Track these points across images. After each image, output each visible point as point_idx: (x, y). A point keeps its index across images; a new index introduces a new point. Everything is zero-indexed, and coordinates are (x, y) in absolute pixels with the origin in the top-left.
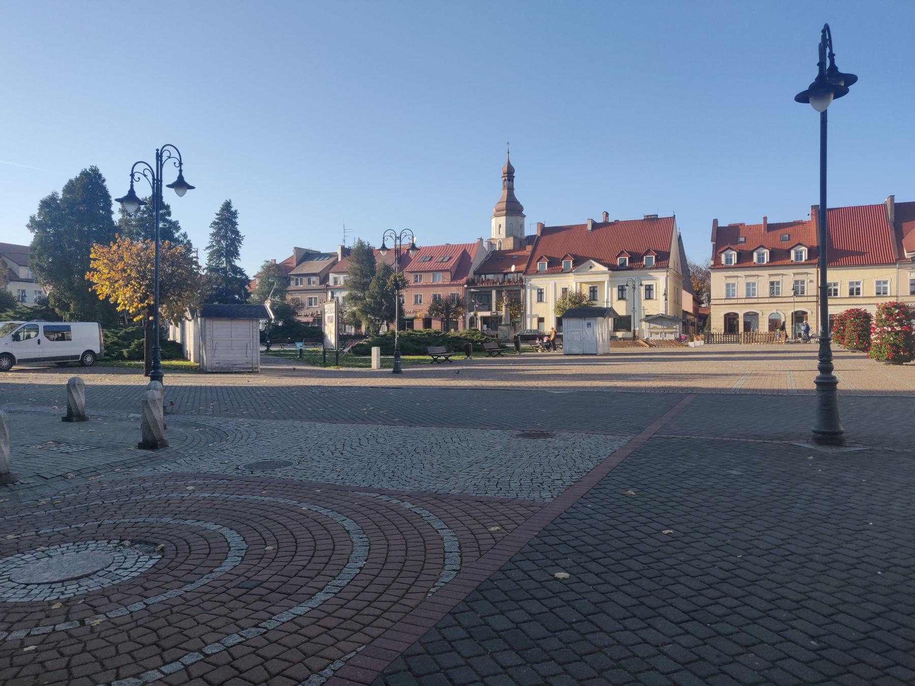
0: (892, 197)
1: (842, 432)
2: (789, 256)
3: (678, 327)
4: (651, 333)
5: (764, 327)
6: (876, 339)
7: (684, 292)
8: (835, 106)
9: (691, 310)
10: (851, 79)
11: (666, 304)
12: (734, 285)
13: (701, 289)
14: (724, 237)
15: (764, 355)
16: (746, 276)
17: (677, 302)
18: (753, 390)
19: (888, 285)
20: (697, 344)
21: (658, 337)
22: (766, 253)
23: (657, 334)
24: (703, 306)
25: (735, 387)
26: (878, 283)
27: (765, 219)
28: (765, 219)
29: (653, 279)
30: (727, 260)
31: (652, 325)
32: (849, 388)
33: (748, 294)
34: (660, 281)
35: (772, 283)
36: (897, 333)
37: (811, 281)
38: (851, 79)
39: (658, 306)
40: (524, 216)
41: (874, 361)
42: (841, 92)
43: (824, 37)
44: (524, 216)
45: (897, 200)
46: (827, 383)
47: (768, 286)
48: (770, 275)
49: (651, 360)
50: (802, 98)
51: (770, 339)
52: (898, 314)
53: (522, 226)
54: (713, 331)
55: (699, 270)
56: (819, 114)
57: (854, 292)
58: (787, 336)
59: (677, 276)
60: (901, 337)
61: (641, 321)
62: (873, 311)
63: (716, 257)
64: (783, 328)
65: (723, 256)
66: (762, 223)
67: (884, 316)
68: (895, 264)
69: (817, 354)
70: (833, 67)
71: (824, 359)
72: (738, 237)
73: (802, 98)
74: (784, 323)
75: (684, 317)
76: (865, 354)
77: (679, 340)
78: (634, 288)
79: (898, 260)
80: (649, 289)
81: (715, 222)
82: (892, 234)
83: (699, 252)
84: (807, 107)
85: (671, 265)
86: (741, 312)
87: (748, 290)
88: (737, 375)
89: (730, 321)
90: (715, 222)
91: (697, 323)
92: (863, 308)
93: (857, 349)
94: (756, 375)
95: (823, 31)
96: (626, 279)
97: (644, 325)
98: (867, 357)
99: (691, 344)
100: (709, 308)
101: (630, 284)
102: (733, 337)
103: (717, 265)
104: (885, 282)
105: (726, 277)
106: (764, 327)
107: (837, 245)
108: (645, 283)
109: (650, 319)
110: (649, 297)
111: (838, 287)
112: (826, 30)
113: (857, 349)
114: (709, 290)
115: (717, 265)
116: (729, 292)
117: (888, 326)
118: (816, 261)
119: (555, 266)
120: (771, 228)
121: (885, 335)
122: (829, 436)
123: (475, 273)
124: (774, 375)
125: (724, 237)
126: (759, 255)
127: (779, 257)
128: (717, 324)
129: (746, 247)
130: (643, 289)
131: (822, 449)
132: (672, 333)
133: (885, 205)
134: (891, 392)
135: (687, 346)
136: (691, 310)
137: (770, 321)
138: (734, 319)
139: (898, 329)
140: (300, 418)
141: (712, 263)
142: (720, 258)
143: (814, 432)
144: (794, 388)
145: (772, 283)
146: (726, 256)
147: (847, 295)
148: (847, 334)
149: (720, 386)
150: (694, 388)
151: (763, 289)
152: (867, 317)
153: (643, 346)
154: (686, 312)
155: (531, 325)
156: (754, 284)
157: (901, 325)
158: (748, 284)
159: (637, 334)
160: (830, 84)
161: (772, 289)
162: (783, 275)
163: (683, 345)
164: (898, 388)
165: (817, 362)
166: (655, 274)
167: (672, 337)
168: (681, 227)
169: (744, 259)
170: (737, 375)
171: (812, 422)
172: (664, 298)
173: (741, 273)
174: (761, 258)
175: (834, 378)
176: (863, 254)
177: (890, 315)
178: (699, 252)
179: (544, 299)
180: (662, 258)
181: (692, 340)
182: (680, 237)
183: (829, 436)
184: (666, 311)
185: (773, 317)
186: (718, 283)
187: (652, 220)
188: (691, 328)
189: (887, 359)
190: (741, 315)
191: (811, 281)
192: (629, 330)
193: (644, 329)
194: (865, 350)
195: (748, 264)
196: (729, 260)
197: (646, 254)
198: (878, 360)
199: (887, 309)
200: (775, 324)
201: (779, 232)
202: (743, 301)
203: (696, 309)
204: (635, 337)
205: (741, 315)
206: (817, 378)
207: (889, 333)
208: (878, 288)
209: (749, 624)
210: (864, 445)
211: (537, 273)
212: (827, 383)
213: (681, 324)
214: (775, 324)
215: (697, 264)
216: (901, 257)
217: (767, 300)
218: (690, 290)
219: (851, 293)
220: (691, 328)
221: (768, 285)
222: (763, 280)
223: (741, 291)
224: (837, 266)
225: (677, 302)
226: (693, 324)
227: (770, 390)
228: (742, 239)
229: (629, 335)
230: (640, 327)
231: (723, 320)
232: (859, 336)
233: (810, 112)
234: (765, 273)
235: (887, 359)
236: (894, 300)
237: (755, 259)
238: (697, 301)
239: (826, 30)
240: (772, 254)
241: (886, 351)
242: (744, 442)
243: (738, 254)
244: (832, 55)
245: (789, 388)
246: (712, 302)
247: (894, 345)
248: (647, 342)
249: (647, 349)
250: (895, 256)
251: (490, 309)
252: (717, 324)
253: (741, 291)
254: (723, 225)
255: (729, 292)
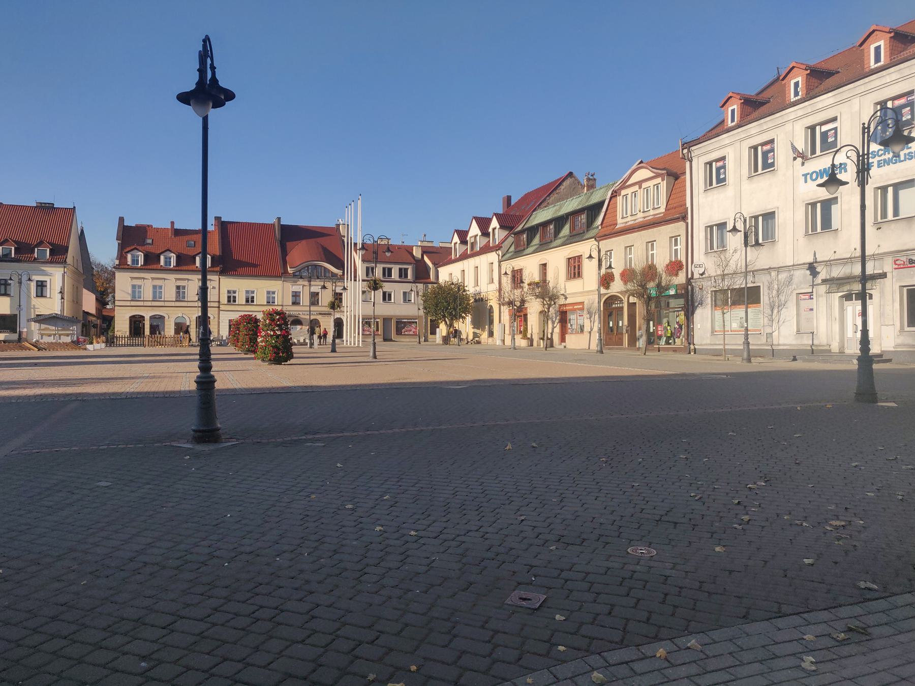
0: (279, 219)
1: (218, 429)
2: (194, 262)
3: (75, 329)
4: (42, 335)
5: (169, 330)
6: (262, 342)
7: (85, 291)
8: (214, 114)
9: (93, 311)
10: (230, 96)
11: (63, 303)
12: (140, 287)
13: (106, 289)
14: (131, 237)
15: (188, 357)
16: (153, 279)
17: (77, 301)
18: (146, 393)
19: (276, 295)
20: (97, 347)
21: (51, 340)
22: (173, 257)
23: (50, 336)
24: (108, 307)
25: (128, 390)
26: (268, 293)
27: (172, 223)
28: (172, 223)
29: (47, 275)
30: (133, 261)
31: (43, 326)
32: (236, 387)
33: (154, 296)
34: (56, 277)
35: (178, 287)
36: (278, 336)
37: (214, 288)
38: (230, 96)
39: (52, 305)
41: (259, 361)
42: (218, 104)
43: (205, 46)
45: (284, 222)
46: (206, 382)
47: (174, 290)
48: (177, 279)
49: (36, 365)
50: (184, 98)
51: (177, 342)
52: (278, 320)
54: (117, 334)
55: (104, 269)
56: (201, 119)
57: (250, 300)
58: (190, 340)
59: (76, 272)
60: (281, 339)
61: (29, 321)
62: (260, 316)
63: (122, 257)
64: (187, 332)
65: (129, 257)
67: (268, 322)
68: (280, 277)
69: (212, 357)
70: (214, 79)
71: (204, 358)
72: (145, 238)
73: (184, 98)
74: (188, 326)
75: (85, 318)
76: (253, 356)
77: (76, 344)
78: (20, 283)
79: (282, 274)
80: (41, 285)
81: (121, 220)
82: (279, 250)
83: (104, 251)
84: (188, 111)
85: (69, 260)
86: (147, 314)
87: (154, 293)
88: (133, 378)
89: (136, 324)
90: (121, 220)
91: (99, 325)
92: (254, 314)
93: (249, 351)
94: (154, 377)
95: (204, 41)
96: (10, 272)
97: (34, 326)
98: (254, 358)
99: (89, 347)
100: (113, 310)
101: (15, 278)
102: (138, 340)
103: (122, 265)
104: (274, 293)
105: (132, 278)
106: (169, 330)
107: (236, 256)
108: (36, 278)
109: (41, 319)
110: (41, 293)
111: (236, 295)
112: (206, 40)
113: (249, 351)
114: (114, 291)
115: (122, 265)
116: (134, 294)
117: (272, 330)
118: (218, 269)
120: (178, 233)
121: (269, 339)
122: (207, 434)
124: (171, 377)
125: (131, 237)
126: (166, 258)
127: (184, 262)
128: (122, 327)
129: (150, 249)
130: (33, 285)
131: (200, 448)
132: (68, 335)
133: (274, 225)
134: (267, 389)
135: (86, 349)
136: (93, 311)
137: (176, 324)
138: (140, 322)
139: (278, 333)
141: (117, 262)
142: (126, 258)
143: (194, 431)
144: (187, 389)
145: (178, 287)
146: (133, 256)
147: (244, 302)
148: (241, 338)
149: (111, 391)
150: (80, 394)
151: (169, 293)
152: (256, 321)
153: (30, 349)
154: (88, 313)
156: (161, 287)
157: (281, 330)
158: (155, 287)
159: (24, 336)
160: (208, 93)
161: (178, 293)
162: (188, 280)
163: (80, 348)
164: (274, 385)
165: (198, 363)
166: (48, 269)
167: (68, 340)
168: (82, 220)
169: (151, 261)
170: (133, 378)
171: (190, 421)
172: (60, 296)
173: (148, 275)
174: (168, 262)
175: (213, 376)
176: (255, 266)
177: (272, 320)
178: (104, 251)
180: (58, 253)
181: (92, 343)
182: (82, 231)
183: (207, 434)
184: (62, 310)
185: (178, 321)
186: (123, 283)
187: (46, 209)
188: (93, 330)
189: (270, 360)
190: (147, 318)
191: (214, 288)
192: (14, 330)
193: (34, 332)
194: (254, 352)
195: (154, 267)
196: (135, 261)
197: (38, 245)
198: (263, 360)
199: (270, 315)
200: (181, 328)
201: (185, 238)
202: (149, 304)
203: (99, 310)
204: (20, 339)
206: (198, 377)
207: (271, 336)
208: (268, 298)
209: (72, 667)
210: (238, 440)
212: (206, 382)
213: (80, 325)
214: (181, 328)
215: (103, 263)
216: (286, 272)
217: (173, 304)
218: (93, 290)
219: (247, 301)
220: (93, 330)
221: (175, 288)
222: (169, 283)
223: (148, 293)
224: (233, 275)
225: (77, 301)
226: (95, 326)
227: (163, 393)
228: (149, 241)
229: (15, 337)
230: (29, 328)
231: (128, 322)
232: (250, 339)
233: (189, 115)
234: (172, 277)
235: (270, 360)
236: (279, 308)
237: (162, 263)
238: (102, 302)
239: (206, 40)
240: (179, 258)
241: (270, 353)
242: (123, 449)
243: (145, 256)
244: (213, 68)
245: (183, 389)
246: (117, 303)
247: (275, 347)
248: (35, 345)
249: (35, 352)
250: (281, 271)
252: (122, 327)
253: (147, 293)
255: (134, 294)
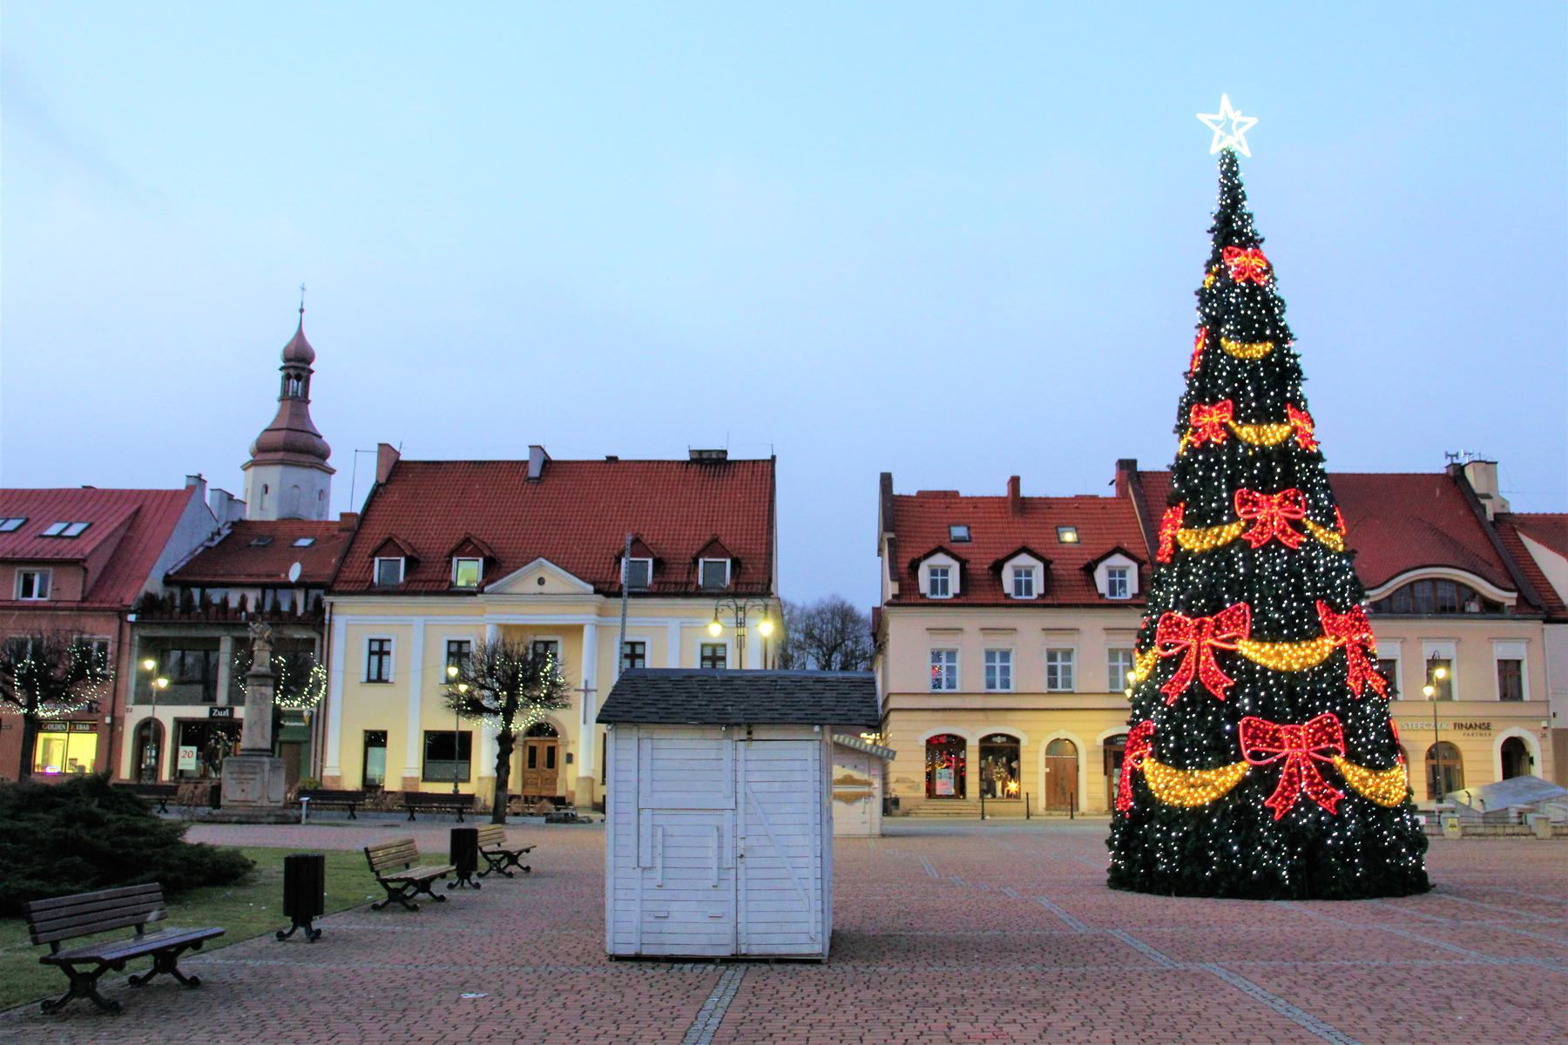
14: (909, 523)
28: (1015, 482)
40: (331, 472)
44: (331, 472)
53: (323, 494)
66: (1003, 491)
103: (907, 595)
119: (426, 579)
123: (168, 581)
125: (909, 523)
140: (803, 688)
155: (341, 765)
179: (384, 692)
187: (710, 463)
205: (973, 745)
211: (370, 589)
223: (971, 674)
251: (209, 698)
254: (905, 492)
